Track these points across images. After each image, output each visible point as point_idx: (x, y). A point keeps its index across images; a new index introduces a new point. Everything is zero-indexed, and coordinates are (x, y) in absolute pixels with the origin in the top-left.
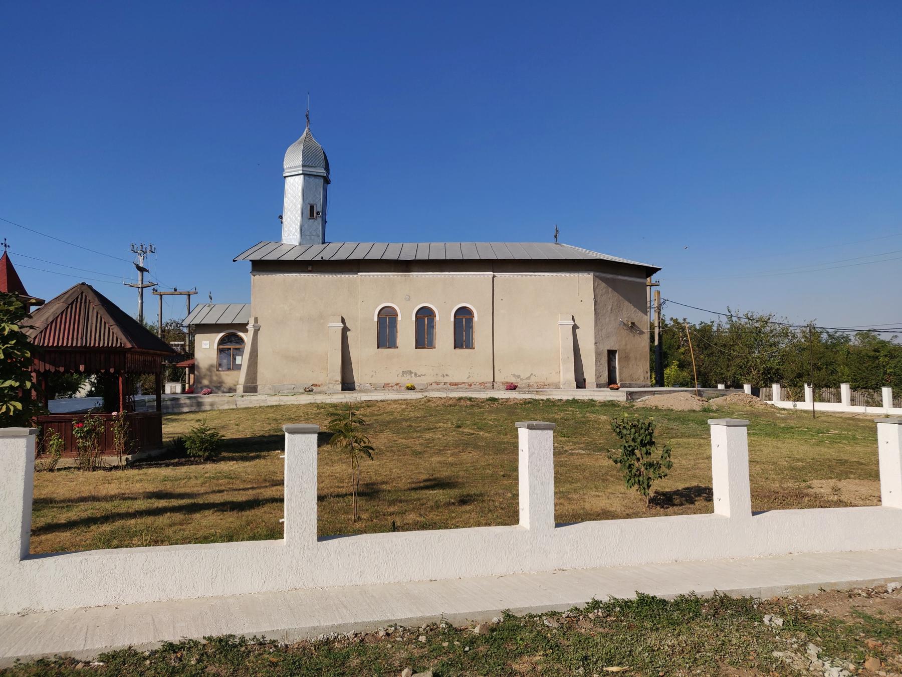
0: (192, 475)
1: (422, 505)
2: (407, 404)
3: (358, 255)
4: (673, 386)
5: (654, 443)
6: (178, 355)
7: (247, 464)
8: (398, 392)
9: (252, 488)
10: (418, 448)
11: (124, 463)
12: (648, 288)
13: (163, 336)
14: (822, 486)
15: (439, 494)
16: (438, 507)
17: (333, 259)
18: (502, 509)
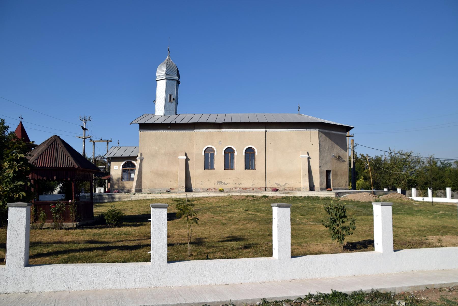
1: (225, 249)
3: (194, 120)
4: (361, 189)
5: (346, 217)
6: (103, 173)
7: (136, 228)
8: (215, 192)
9: (138, 240)
10: (225, 221)
11: (75, 226)
12: (347, 138)
13: (95, 163)
14: (432, 239)
15: (234, 244)
16: (233, 250)
18: (266, 251)
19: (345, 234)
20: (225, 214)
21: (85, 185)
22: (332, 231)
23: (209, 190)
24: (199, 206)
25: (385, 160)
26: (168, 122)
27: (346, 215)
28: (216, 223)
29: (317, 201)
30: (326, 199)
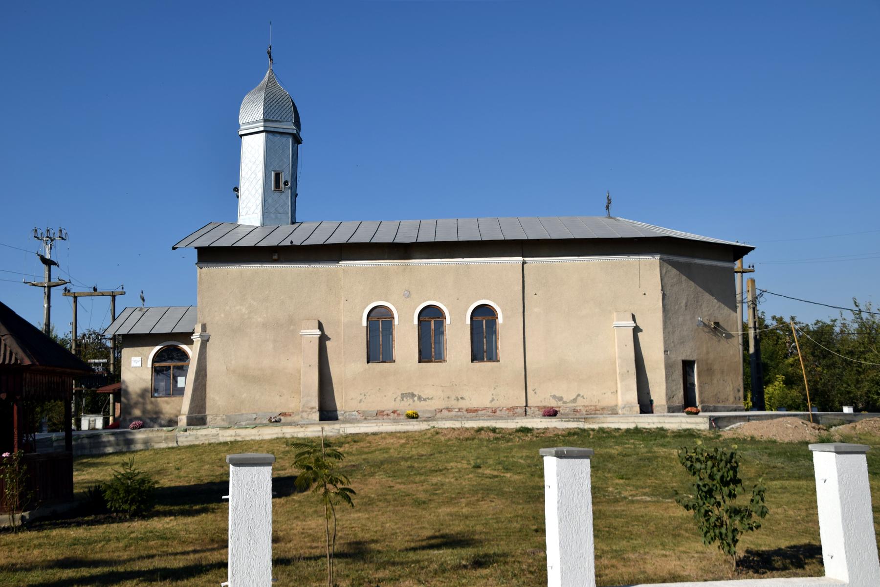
0: (112, 536)
1: (422, 568)
2: (408, 438)
4: (778, 409)
5: (739, 481)
6: (100, 376)
7: (189, 520)
8: (395, 421)
9: (195, 552)
10: (422, 496)
12: (738, 276)
13: (78, 352)
15: (448, 556)
16: (444, 571)
17: (305, 243)
18: (531, 573)
19: (739, 528)
20: (423, 478)
21: (50, 410)
22: (703, 519)
23: (380, 414)
24: (354, 458)
25: (842, 332)
26: (272, 241)
27: (739, 476)
28: (400, 500)
29: (661, 441)
30: (685, 436)
